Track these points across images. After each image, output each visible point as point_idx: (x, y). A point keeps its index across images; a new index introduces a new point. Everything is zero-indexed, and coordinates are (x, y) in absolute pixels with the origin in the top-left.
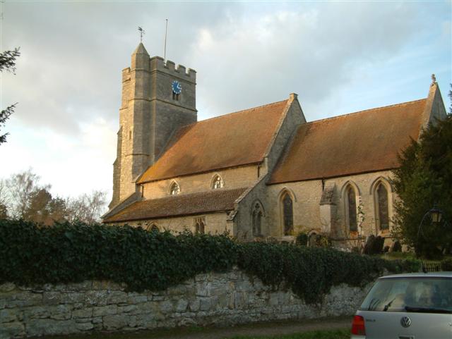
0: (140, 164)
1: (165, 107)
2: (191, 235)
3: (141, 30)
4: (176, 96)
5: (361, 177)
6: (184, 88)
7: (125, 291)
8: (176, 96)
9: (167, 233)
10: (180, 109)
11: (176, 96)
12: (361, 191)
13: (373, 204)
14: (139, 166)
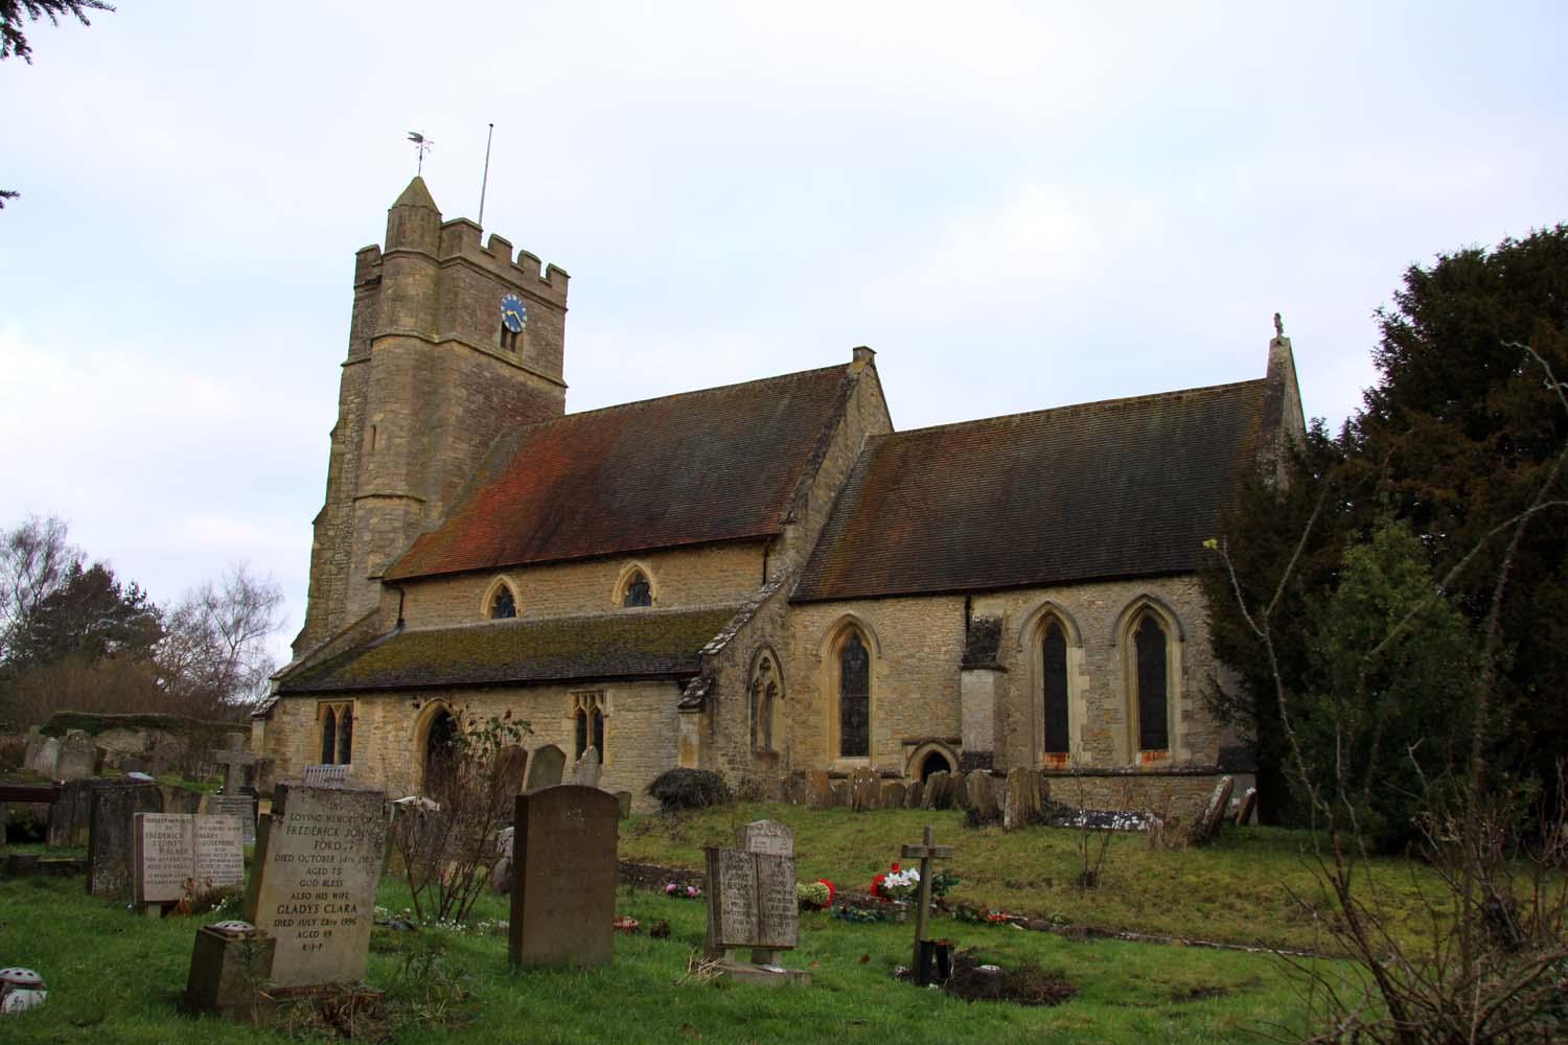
0: (397, 524)
1: (478, 365)
3: (419, 139)
4: (509, 337)
5: (1086, 594)
6: (534, 319)
8: (509, 337)
10: (521, 377)
11: (509, 336)
12: (1085, 633)
13: (1121, 675)
14: (394, 530)
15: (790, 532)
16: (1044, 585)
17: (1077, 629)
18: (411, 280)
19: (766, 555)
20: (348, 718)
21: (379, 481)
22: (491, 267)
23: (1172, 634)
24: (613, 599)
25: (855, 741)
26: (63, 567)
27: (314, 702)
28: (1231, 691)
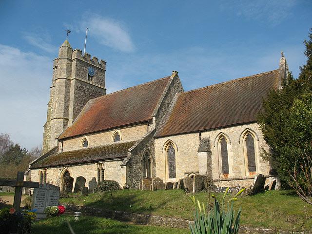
16: (220, 128)
17: (229, 139)
20: (46, 174)
23: (255, 139)
25: (172, 175)
26: (9, 145)
27: (38, 170)
28: (267, 151)
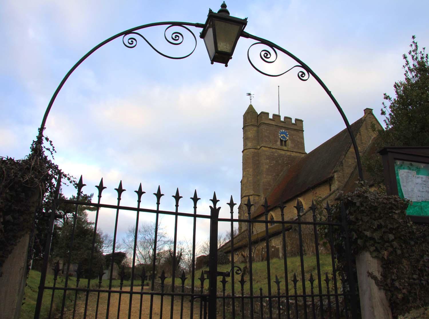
2: (142, 264)
3: (249, 94)
6: (291, 135)
7: (406, 79)
8: (283, 142)
9: (46, 157)
10: (289, 153)
11: (283, 142)
15: (336, 176)
18: (249, 133)
19: (330, 186)
21: (246, 192)
22: (273, 124)
24: (295, 212)
